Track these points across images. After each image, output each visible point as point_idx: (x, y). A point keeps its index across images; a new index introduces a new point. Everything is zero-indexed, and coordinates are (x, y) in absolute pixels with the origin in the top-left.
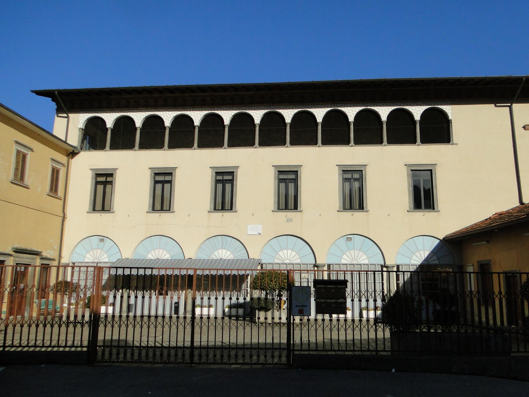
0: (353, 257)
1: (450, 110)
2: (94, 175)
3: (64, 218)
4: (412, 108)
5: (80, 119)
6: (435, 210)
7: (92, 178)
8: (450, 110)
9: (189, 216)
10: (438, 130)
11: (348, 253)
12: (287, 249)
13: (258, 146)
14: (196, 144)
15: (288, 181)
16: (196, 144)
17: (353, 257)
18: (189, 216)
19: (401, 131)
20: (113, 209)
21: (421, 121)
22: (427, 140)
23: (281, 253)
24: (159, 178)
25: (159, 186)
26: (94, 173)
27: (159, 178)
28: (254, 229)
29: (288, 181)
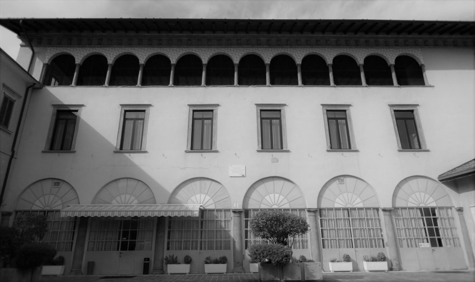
0: (347, 201)
1: (420, 56)
2: (56, 111)
3: (12, 157)
4: (391, 53)
5: (49, 54)
6: (284, 149)
7: (53, 115)
8: (420, 56)
9: (236, 154)
10: (411, 74)
11: (341, 196)
12: (274, 193)
13: (107, 86)
14: (171, 82)
15: (337, 119)
16: (171, 82)
17: (347, 201)
18: (236, 154)
19: (378, 74)
20: (74, 148)
21: (365, 66)
22: (403, 82)
23: (267, 198)
24: (265, 115)
25: (266, 122)
26: (56, 109)
27: (197, 115)
28: (235, 169)
29: (337, 119)
